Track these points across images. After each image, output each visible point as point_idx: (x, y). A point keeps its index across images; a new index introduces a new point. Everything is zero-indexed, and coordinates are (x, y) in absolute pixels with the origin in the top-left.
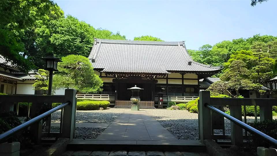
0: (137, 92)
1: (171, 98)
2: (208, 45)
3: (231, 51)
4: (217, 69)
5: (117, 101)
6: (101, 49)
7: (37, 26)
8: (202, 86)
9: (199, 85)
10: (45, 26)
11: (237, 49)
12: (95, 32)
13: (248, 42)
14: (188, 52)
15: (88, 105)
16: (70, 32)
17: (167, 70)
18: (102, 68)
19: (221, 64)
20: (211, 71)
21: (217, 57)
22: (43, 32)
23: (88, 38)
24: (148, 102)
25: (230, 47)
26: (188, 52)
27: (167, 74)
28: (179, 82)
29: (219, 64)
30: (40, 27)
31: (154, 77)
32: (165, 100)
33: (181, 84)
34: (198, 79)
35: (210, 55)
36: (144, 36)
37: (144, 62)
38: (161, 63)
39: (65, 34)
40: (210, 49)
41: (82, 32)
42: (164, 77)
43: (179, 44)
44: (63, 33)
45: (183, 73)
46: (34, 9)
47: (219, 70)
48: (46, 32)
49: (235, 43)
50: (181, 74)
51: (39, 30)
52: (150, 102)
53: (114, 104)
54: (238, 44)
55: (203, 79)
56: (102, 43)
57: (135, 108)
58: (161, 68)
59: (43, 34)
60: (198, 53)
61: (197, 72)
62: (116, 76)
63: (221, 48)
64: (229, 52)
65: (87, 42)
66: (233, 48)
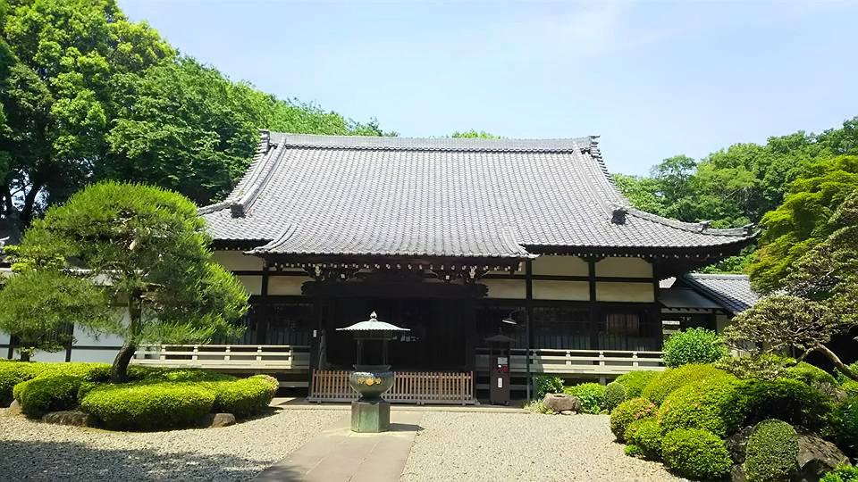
0: (382, 341)
1: (543, 357)
2: (683, 158)
3: (767, 176)
4: (735, 240)
5: (317, 375)
6: (280, 169)
7: (60, 92)
8: (670, 309)
9: (656, 305)
10: (88, 93)
11: (787, 170)
12: (273, 114)
13: (825, 145)
14: (612, 179)
15: (153, 409)
16: (176, 111)
17: (525, 246)
18: (263, 240)
19: (731, 222)
20: (708, 247)
21: (715, 200)
22: (82, 113)
23: (246, 132)
24: (446, 377)
25: (760, 164)
26: (612, 179)
27: (528, 262)
28: (579, 294)
29: (724, 224)
30: (73, 96)
31: (472, 274)
32: (519, 366)
33: (587, 297)
34: (655, 281)
35: (691, 192)
36: (461, 134)
37: (438, 214)
38: (504, 218)
39: (159, 119)
40: (689, 172)
41: (224, 111)
42: (512, 271)
43: (576, 148)
44: (153, 117)
45: (592, 254)
46: (55, 35)
47: (740, 242)
48: (90, 113)
49: (778, 148)
50: (585, 260)
51: (66, 105)
52: (454, 377)
53: (306, 384)
54: (791, 153)
55: (672, 280)
56: (288, 147)
57: (366, 418)
58: (504, 236)
59: (79, 121)
60: (647, 187)
61: (651, 249)
62: (318, 272)
63: (728, 167)
64: (759, 180)
65: (243, 148)
66: (773, 165)
